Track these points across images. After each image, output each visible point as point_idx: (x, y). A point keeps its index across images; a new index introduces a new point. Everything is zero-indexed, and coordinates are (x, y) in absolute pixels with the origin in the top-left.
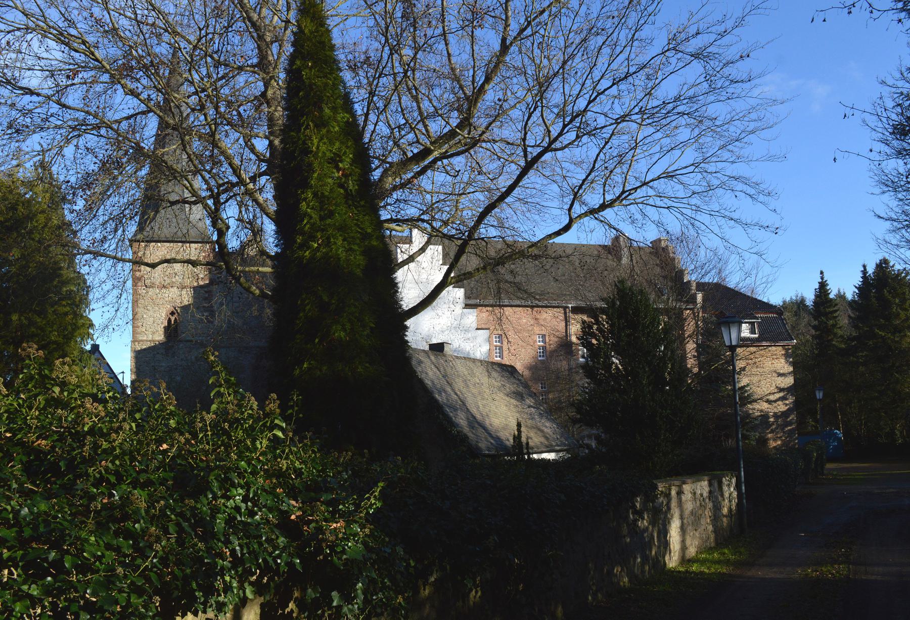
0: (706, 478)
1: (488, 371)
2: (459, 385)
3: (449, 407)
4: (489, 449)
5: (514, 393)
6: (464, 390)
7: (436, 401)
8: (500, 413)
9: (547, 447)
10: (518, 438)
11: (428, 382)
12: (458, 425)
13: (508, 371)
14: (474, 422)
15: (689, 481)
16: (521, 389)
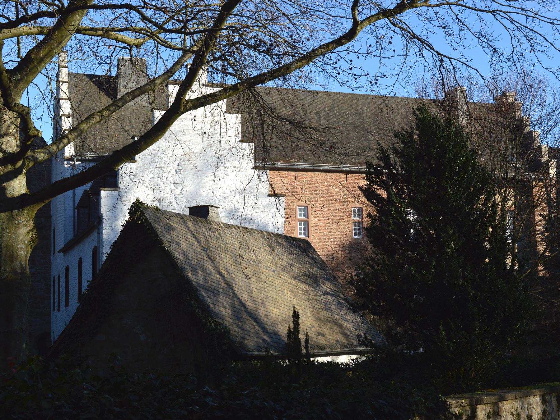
0: (537, 392)
1: (270, 246)
2: (226, 261)
3: (207, 290)
4: (258, 348)
5: (305, 275)
6: (233, 269)
7: (188, 281)
8: (280, 298)
9: (345, 347)
10: (294, 332)
11: (178, 256)
12: (216, 315)
13: (299, 247)
14: (242, 311)
15: (509, 396)
16: (315, 270)
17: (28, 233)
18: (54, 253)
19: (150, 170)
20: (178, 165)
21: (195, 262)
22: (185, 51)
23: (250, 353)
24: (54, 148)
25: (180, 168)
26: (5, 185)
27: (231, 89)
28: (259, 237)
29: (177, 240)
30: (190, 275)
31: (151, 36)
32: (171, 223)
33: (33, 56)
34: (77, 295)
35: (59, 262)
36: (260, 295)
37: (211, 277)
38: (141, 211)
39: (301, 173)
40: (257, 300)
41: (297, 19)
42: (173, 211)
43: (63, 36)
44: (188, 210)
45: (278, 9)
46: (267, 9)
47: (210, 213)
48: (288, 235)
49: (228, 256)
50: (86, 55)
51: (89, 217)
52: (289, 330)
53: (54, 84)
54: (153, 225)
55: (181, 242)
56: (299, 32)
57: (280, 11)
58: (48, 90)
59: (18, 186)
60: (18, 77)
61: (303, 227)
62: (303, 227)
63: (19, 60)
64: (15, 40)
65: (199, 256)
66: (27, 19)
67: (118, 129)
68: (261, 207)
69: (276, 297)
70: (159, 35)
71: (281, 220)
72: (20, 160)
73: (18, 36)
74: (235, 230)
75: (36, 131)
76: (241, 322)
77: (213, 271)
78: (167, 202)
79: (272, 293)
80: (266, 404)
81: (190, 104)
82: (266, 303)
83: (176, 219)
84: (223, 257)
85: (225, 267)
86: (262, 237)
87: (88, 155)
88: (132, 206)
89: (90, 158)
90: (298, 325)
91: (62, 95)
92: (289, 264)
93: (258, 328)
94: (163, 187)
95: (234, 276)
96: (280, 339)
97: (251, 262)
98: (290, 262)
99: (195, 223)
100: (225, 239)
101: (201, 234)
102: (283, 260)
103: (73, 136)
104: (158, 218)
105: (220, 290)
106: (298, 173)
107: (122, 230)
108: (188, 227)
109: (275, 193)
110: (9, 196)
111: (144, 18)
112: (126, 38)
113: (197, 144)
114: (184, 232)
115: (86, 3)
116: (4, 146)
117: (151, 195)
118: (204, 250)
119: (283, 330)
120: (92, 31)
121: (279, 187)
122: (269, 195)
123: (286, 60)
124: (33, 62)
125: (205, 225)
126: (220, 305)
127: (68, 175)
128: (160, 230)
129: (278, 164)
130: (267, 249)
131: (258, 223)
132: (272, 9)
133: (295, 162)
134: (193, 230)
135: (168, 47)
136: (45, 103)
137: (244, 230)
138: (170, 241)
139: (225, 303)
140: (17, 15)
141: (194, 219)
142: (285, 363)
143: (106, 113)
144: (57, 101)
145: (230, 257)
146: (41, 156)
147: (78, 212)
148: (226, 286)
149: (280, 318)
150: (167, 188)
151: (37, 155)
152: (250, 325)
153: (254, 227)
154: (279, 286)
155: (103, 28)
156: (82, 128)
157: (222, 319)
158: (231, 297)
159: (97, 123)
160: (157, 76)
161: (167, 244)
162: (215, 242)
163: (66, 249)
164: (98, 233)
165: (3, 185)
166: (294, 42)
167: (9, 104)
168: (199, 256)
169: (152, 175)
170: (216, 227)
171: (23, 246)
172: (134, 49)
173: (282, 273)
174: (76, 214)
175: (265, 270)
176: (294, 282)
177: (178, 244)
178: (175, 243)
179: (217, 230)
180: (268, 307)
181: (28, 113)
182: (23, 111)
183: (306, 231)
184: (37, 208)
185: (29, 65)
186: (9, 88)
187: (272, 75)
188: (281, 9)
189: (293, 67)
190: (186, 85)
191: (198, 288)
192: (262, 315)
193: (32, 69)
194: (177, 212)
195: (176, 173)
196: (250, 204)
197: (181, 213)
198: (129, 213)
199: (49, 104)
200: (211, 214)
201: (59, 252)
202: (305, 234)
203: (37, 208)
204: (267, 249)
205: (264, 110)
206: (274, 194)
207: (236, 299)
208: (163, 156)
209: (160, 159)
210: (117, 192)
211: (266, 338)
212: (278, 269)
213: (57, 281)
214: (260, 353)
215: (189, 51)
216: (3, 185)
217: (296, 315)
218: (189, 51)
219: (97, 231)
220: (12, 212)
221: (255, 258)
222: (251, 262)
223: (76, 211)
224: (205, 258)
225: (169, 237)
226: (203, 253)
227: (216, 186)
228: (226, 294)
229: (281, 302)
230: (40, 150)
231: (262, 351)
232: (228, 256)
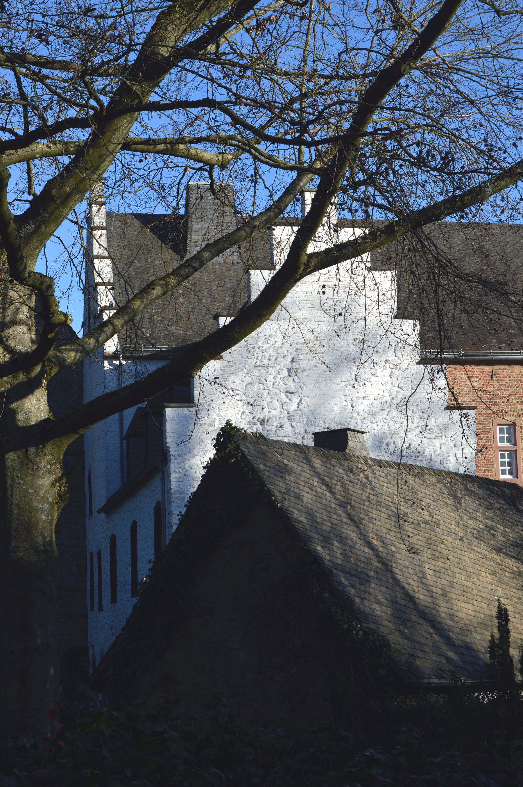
1: (454, 496)
2: (379, 524)
3: (349, 574)
4: (439, 672)
5: (515, 545)
6: (391, 537)
7: (317, 559)
10: (501, 643)
11: (299, 516)
12: (366, 617)
13: (502, 496)
14: (410, 609)
17: (53, 484)
18: (91, 513)
19: (246, 371)
20: (292, 361)
21: (326, 526)
22: (301, 171)
23: (426, 681)
24: (92, 342)
25: (295, 366)
26: (14, 406)
27: (382, 232)
28: (435, 480)
29: (297, 490)
30: (319, 548)
31: (246, 147)
32: (286, 462)
33: (54, 192)
34: (129, 583)
35: (99, 530)
36: (439, 580)
37: (354, 551)
38: (235, 442)
39: (502, 367)
40: (435, 590)
41: (490, 107)
42: (286, 440)
43: (101, 156)
44: (311, 437)
45: (458, 91)
46: (439, 92)
47: (350, 442)
48: (482, 475)
49: (382, 514)
50: (137, 185)
51: (148, 454)
52: (492, 641)
53: (85, 232)
54: (256, 466)
55: (302, 493)
56: (494, 127)
57: (461, 94)
58: (78, 245)
59: (36, 407)
60: (30, 227)
61: (507, 460)
62: (507, 460)
63: (31, 198)
64: (24, 165)
65: (334, 516)
66: (46, 131)
67: (190, 303)
68: (435, 429)
69: (467, 584)
70: (257, 146)
71: (469, 452)
72: (37, 364)
73: (28, 160)
74: (394, 471)
75: (62, 316)
76: (408, 628)
77: (359, 541)
78: (275, 424)
79: (460, 578)
80: (474, 779)
81: (313, 262)
82: (449, 595)
83: (293, 454)
84: (374, 516)
85: (378, 533)
86: (438, 481)
87: (144, 349)
88: (219, 434)
89: (146, 354)
90: (508, 632)
91: (97, 250)
92: (486, 526)
93: (437, 637)
94: (268, 399)
95: (393, 549)
96: (476, 657)
97: (423, 525)
98: (489, 523)
99: (324, 459)
100: (377, 485)
101: (336, 478)
102: (476, 519)
103: (121, 322)
104: (264, 454)
105: (372, 573)
106: (496, 367)
107: (203, 476)
108: (313, 467)
109: (458, 403)
110: (21, 424)
111: (236, 121)
112: (203, 154)
113: (321, 324)
114: (308, 476)
115: (141, 102)
116: (11, 343)
117: (247, 412)
118: (341, 505)
119: (481, 640)
120: (148, 146)
121: (464, 393)
122: (448, 408)
123: (476, 180)
124: (54, 201)
125: (343, 462)
126: (372, 599)
127: (112, 386)
128: (267, 473)
129: (462, 354)
130: (449, 502)
131: (431, 456)
132: (446, 91)
133: (490, 349)
134: (322, 472)
135: (272, 166)
136: (73, 267)
137: (407, 468)
138: (285, 491)
139: (380, 597)
140: (27, 124)
141: (324, 454)
142: (486, 698)
143: (173, 281)
144: (89, 258)
145: (385, 516)
146: (71, 356)
147: (128, 445)
148: (380, 566)
149: (475, 620)
150: (275, 401)
151: (64, 354)
152: (424, 632)
153: (424, 464)
154: (471, 565)
155: (166, 139)
156: (135, 307)
157: (375, 623)
158: (389, 585)
159: (159, 297)
160: (255, 214)
161: (279, 497)
162: (360, 492)
163: (111, 507)
164: (163, 479)
165: (12, 406)
166: (491, 150)
167: (18, 272)
168: (334, 516)
169: (248, 380)
170: (360, 466)
171: (46, 507)
172: (216, 172)
173: (475, 542)
174: (125, 448)
175: (446, 538)
176: (498, 558)
177: (298, 497)
178: (292, 494)
179: (363, 471)
180: (454, 602)
181: (50, 286)
182: (42, 283)
183: (514, 471)
184: (66, 443)
185: (47, 207)
186: (20, 247)
187: (455, 204)
188: (462, 90)
189: (489, 190)
190: (307, 228)
191: (334, 571)
192: (443, 615)
193: (53, 212)
194: (293, 441)
195: (290, 376)
196: (416, 425)
197: (299, 442)
198: (215, 446)
199: (79, 269)
200: (351, 443)
201: (99, 512)
202: (510, 473)
203: (66, 443)
204: (449, 502)
205: (441, 265)
206: (455, 406)
207: (398, 589)
208: (266, 346)
209: (262, 351)
210: (193, 409)
211: (450, 654)
212: (469, 536)
213: (96, 560)
214: (442, 681)
215: (311, 170)
216: (12, 406)
217: (503, 616)
218: (311, 170)
219: (160, 476)
220: (26, 451)
221: (428, 518)
222: (423, 525)
223: (125, 442)
224: (345, 520)
225: (282, 485)
226: (340, 511)
227: (357, 395)
228: (381, 580)
229: (475, 592)
230: (68, 347)
231: (445, 679)
232: (382, 514)
